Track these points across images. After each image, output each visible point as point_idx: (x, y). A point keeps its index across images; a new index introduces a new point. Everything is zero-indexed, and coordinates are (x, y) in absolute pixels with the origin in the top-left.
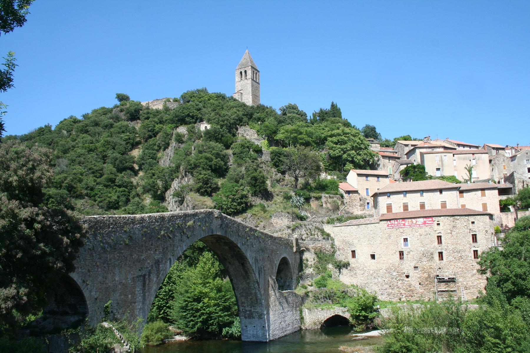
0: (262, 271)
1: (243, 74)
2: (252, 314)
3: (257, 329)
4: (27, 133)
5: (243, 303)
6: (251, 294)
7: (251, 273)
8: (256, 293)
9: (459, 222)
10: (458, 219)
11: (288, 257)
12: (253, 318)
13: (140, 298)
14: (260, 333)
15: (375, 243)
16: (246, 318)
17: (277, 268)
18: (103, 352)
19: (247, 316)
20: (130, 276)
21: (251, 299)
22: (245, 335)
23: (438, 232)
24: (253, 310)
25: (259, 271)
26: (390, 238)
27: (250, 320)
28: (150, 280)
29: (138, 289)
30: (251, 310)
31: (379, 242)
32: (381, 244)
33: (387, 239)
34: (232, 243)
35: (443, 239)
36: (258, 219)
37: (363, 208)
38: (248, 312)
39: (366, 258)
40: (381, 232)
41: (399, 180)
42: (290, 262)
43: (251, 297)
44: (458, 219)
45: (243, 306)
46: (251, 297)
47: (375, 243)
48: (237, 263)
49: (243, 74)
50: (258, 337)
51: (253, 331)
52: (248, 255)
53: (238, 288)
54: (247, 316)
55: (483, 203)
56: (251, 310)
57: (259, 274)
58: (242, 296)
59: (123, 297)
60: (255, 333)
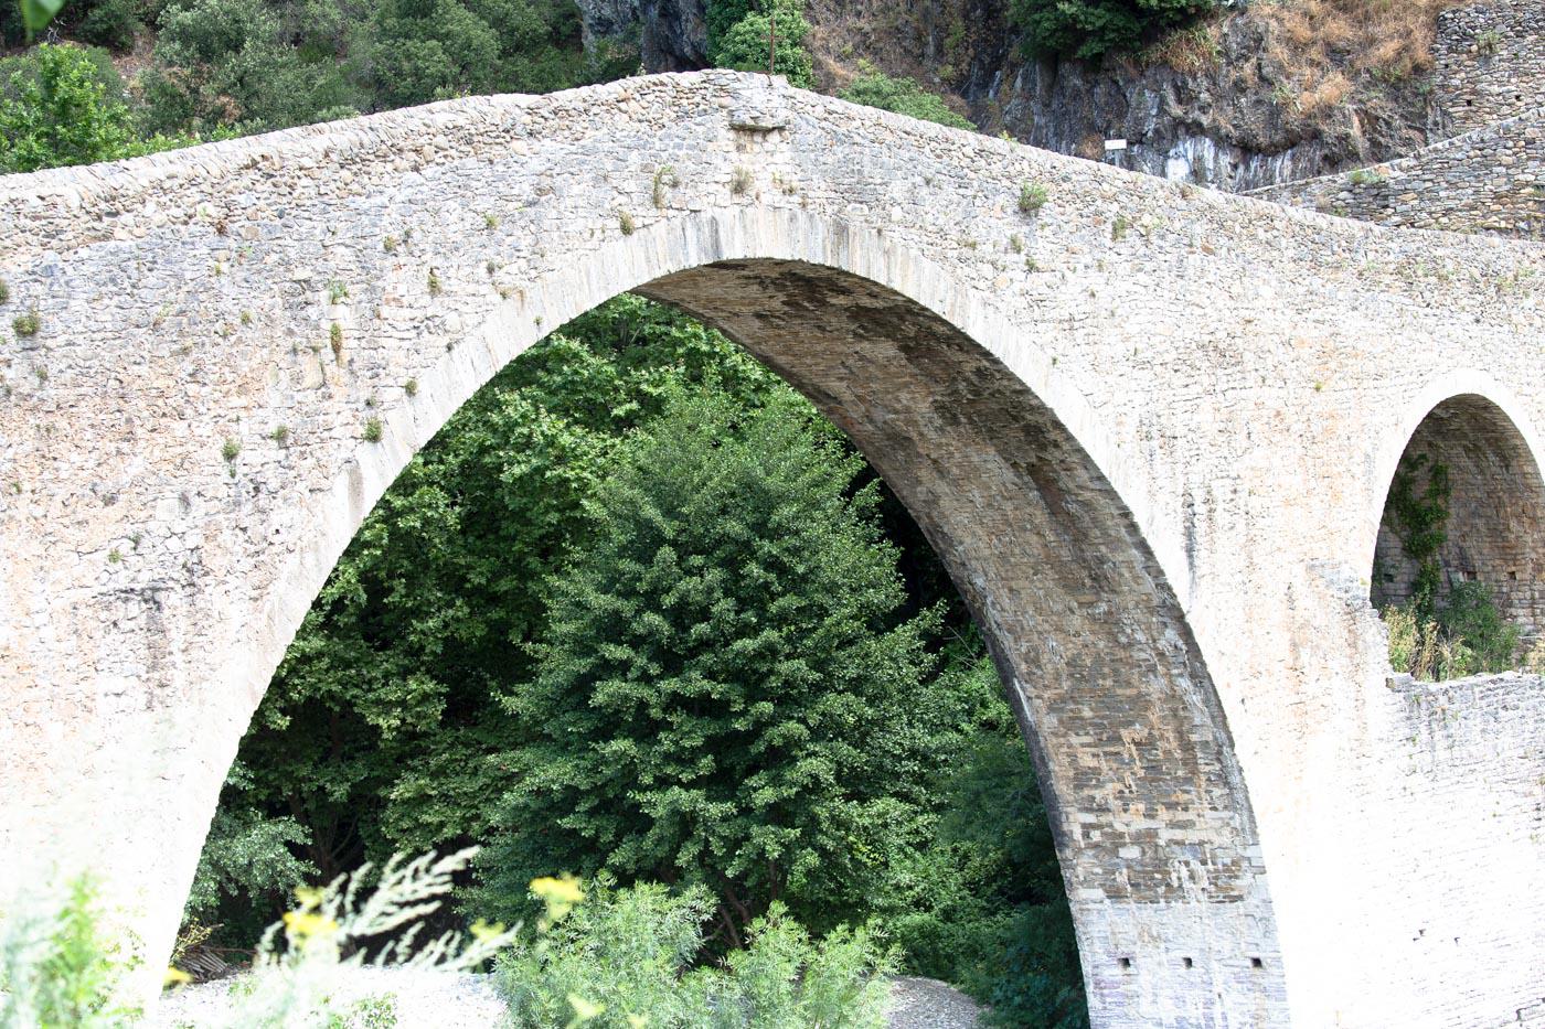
2: (1161, 865)
5: (1082, 778)
8: (1173, 697)
12: (1174, 892)
16: (1115, 894)
25: (1189, 533)
43: (1139, 733)
53: (1033, 660)
58: (1074, 724)
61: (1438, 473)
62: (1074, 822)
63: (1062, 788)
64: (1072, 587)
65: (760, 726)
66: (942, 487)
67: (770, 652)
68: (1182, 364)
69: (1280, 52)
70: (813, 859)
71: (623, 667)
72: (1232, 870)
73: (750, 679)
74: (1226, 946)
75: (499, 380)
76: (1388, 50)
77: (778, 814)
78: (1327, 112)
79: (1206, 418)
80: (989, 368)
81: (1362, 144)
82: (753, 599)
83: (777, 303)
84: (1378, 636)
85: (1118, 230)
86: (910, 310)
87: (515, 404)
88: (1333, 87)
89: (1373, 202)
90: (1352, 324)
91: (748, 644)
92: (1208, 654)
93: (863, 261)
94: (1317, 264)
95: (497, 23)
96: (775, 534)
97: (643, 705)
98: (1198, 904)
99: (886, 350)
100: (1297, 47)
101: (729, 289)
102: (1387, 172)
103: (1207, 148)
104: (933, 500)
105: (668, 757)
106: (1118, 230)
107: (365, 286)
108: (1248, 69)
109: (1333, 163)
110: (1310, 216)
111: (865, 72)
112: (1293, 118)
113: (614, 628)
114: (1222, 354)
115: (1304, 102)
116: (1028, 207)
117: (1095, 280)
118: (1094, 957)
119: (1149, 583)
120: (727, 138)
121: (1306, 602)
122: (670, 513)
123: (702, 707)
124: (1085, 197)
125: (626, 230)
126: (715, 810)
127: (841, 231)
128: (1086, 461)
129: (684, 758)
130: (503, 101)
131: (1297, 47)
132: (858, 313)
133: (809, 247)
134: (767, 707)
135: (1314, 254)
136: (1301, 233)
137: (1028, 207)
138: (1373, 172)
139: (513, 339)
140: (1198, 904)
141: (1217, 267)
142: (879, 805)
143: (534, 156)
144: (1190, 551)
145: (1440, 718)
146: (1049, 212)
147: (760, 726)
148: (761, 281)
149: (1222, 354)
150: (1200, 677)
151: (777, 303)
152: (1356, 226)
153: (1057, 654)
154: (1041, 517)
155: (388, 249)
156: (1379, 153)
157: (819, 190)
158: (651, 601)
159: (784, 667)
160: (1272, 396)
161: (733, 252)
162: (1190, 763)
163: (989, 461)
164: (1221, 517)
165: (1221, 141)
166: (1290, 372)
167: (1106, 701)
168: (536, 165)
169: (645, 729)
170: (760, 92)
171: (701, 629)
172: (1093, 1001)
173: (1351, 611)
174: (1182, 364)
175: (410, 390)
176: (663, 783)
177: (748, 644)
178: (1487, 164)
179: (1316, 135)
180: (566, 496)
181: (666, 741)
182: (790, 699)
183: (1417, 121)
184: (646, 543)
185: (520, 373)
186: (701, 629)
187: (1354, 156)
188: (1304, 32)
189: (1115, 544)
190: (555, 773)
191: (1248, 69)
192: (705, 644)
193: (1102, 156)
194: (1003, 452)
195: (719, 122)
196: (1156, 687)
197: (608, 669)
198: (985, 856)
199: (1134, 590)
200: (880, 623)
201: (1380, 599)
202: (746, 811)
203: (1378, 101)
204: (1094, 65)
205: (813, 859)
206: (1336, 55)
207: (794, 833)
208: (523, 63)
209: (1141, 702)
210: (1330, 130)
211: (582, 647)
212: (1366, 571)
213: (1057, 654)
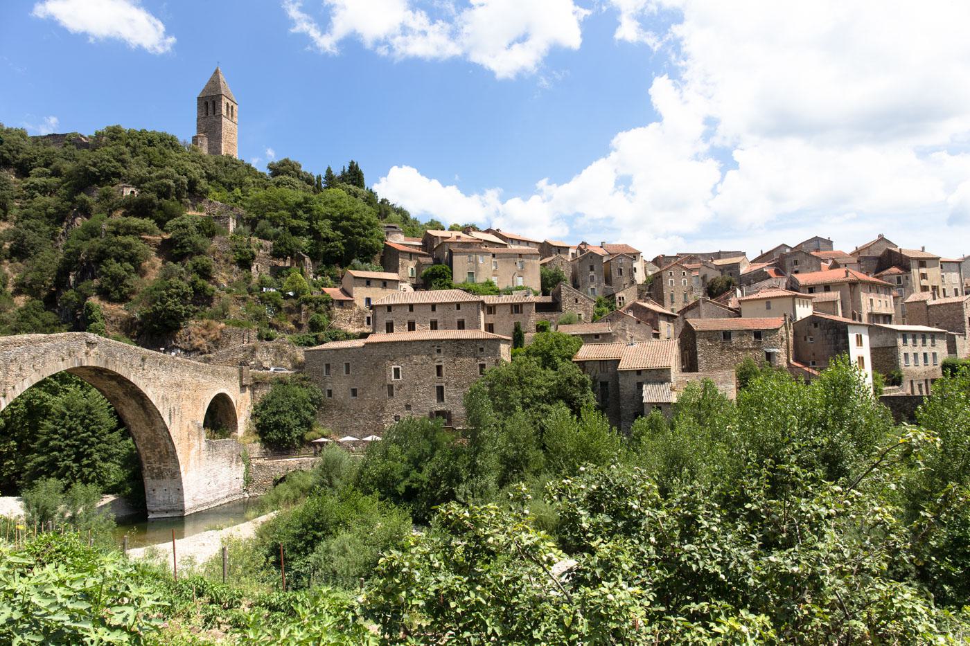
1: (210, 106)
2: (162, 473)
4: (580, 33)
5: (147, 458)
8: (165, 444)
11: (228, 393)
12: (164, 478)
16: (153, 478)
22: (151, 502)
23: (438, 360)
25: (170, 415)
31: (363, 373)
32: (365, 374)
35: (444, 369)
41: (685, 302)
42: (234, 401)
43: (159, 450)
46: (159, 450)
49: (210, 106)
52: (150, 391)
53: (139, 437)
55: (466, 321)
58: (147, 448)
59: (381, 598)
60: (166, 498)
61: (216, 405)
62: (145, 466)
63: (143, 460)
64: (147, 424)
65: (85, 450)
66: (124, 407)
67: (89, 436)
68: (171, 386)
69: (193, 335)
70: (95, 474)
71: (56, 439)
72: (175, 473)
73: (84, 441)
74: (173, 487)
75: (34, 386)
76: (213, 336)
77: (88, 466)
78: (201, 345)
79: (175, 396)
80: (134, 386)
81: (207, 351)
82: (87, 428)
83: (93, 374)
84: (204, 433)
85: (160, 364)
86: (119, 376)
87: (36, 390)
88: (202, 341)
89: (208, 360)
90: (202, 380)
91: (85, 435)
92: (172, 436)
93: (111, 367)
94: (197, 371)
95: (42, 321)
96: (93, 414)
97: (60, 446)
98: (168, 479)
99: (114, 383)
100: (196, 335)
101: (84, 371)
102: (211, 356)
103: (179, 351)
104: (122, 409)
105: (65, 456)
106: (160, 364)
107: (803, 278)
108: (188, 337)
109: (201, 354)
110: (197, 363)
111: (116, 334)
112: (195, 346)
113: (55, 432)
114: (178, 385)
115: (197, 344)
116: (143, 360)
117: (156, 372)
118: (148, 489)
119: (162, 424)
120: (85, 345)
121: (191, 427)
122: (68, 409)
123: (73, 446)
124: (154, 358)
125: (63, 360)
126: (74, 465)
127: (107, 362)
128: (152, 403)
129: (69, 456)
130: (39, 335)
131: (196, 335)
132: (109, 376)
133: (101, 365)
134: (86, 446)
135: (196, 368)
136: (194, 365)
137: (143, 360)
138: (208, 355)
139: (37, 378)
140: (168, 479)
141: (178, 371)
142: (109, 464)
143: (45, 346)
144: (170, 418)
145: (214, 447)
146: (147, 360)
147: (85, 450)
148: (90, 370)
149: (178, 385)
150: (171, 440)
151: (93, 374)
152: (204, 364)
153: (144, 435)
154: (142, 412)
155: (11, 361)
156: (210, 352)
157: (103, 354)
158: (64, 426)
159: (92, 439)
160: (187, 392)
161: (85, 364)
162: (168, 455)
163: (133, 402)
164: (176, 413)
165: (182, 349)
166: (191, 388)
167: (152, 444)
168: (45, 347)
169: (60, 450)
170: (92, 337)
171: (74, 432)
172: (147, 497)
173: (199, 429)
174: (171, 386)
175: (14, 388)
176: (64, 460)
177: (85, 435)
178: (229, 355)
179: (199, 350)
180: (48, 408)
181: (65, 453)
182: (92, 445)
183: (217, 347)
184: (63, 416)
185: (39, 385)
186: (74, 432)
187: (205, 353)
188: (198, 332)
189: (156, 417)
190: (41, 459)
191: (188, 337)
192: (74, 435)
193: (160, 351)
194: (136, 401)
195: (84, 342)
196: (162, 442)
197: (52, 439)
198: (128, 472)
199: (159, 425)
200: (112, 431)
201: (205, 426)
202: (81, 465)
203: (210, 344)
204: (159, 335)
205: (95, 474)
206: (203, 336)
207: (91, 470)
208: (47, 328)
209: (159, 445)
210: (201, 348)
211: (48, 434)
212: (202, 422)
213: (144, 435)
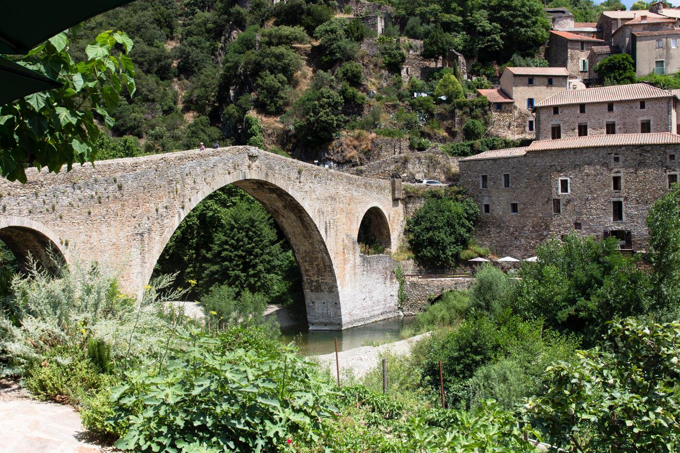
0: (332, 227)
2: (320, 286)
3: (327, 307)
5: (307, 271)
6: (317, 258)
7: (313, 230)
8: (322, 257)
9: (649, 155)
10: (649, 151)
12: (322, 291)
13: (138, 261)
14: (331, 312)
15: (518, 186)
16: (312, 291)
17: (360, 223)
18: (370, 452)
19: (313, 288)
20: (122, 234)
21: (318, 265)
22: (311, 314)
24: (320, 281)
25: (326, 229)
26: (540, 180)
27: (317, 294)
28: (150, 239)
29: (135, 252)
30: (318, 281)
32: (527, 188)
33: (536, 180)
34: (279, 189)
36: (108, 197)
37: (522, 129)
38: (315, 284)
39: (504, 208)
40: (527, 170)
43: (316, 263)
44: (649, 151)
45: (307, 275)
46: (316, 263)
47: (518, 186)
48: (293, 216)
50: (329, 317)
51: (322, 310)
54: (313, 288)
56: (318, 281)
57: (326, 232)
58: (306, 261)
60: (325, 312)
